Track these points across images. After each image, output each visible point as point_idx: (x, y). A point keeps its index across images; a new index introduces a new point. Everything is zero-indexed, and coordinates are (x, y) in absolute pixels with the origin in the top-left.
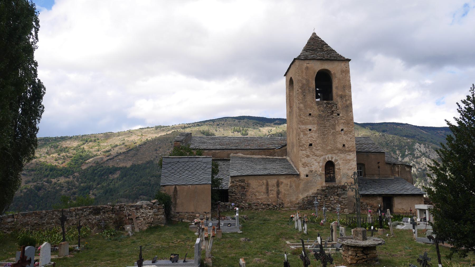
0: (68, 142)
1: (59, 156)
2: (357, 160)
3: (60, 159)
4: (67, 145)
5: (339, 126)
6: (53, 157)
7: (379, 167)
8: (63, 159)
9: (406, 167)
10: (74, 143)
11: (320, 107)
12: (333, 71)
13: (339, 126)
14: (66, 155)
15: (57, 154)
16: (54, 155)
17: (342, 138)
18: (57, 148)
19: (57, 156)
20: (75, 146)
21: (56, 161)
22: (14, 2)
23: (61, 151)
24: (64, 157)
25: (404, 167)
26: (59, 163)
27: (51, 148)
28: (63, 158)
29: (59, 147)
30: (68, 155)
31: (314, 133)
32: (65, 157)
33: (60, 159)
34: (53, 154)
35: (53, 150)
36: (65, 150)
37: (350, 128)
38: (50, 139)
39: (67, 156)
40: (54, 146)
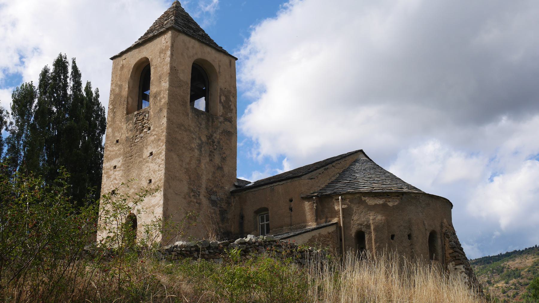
0: (518, 260)
1: (508, 285)
2: (164, 203)
3: (509, 289)
4: (517, 266)
5: (146, 148)
6: (498, 287)
7: (291, 209)
8: (515, 289)
9: (363, 198)
10: (527, 261)
11: (129, 125)
12: (151, 57)
13: (146, 148)
14: (519, 282)
15: (503, 282)
16: (500, 285)
17: (148, 169)
18: (502, 272)
19: (505, 285)
20: (530, 265)
21: (504, 293)
22: (65, 93)
23: (509, 276)
24: (515, 285)
25: (360, 198)
26: (508, 297)
27: (493, 273)
28: (513, 287)
29: (505, 270)
30: (521, 281)
31: (118, 171)
32: (517, 285)
33: (509, 289)
34: (497, 282)
35: (497, 278)
36: (514, 274)
37: (160, 148)
38: (491, 259)
39: (520, 284)
40: (497, 270)
